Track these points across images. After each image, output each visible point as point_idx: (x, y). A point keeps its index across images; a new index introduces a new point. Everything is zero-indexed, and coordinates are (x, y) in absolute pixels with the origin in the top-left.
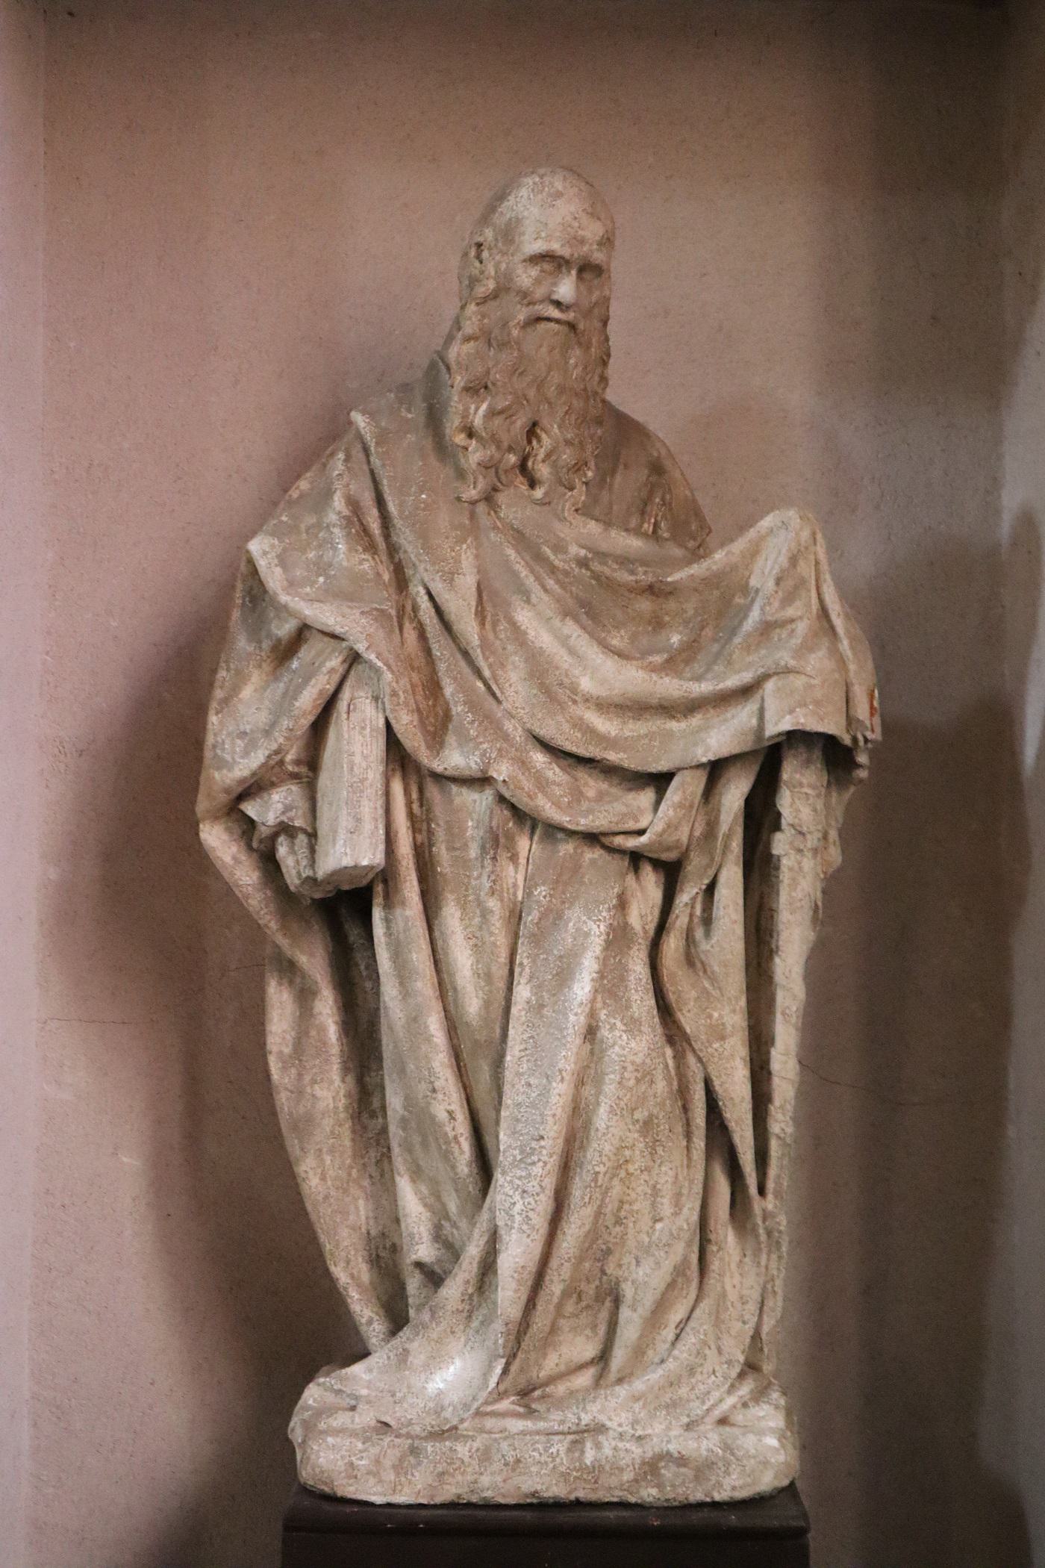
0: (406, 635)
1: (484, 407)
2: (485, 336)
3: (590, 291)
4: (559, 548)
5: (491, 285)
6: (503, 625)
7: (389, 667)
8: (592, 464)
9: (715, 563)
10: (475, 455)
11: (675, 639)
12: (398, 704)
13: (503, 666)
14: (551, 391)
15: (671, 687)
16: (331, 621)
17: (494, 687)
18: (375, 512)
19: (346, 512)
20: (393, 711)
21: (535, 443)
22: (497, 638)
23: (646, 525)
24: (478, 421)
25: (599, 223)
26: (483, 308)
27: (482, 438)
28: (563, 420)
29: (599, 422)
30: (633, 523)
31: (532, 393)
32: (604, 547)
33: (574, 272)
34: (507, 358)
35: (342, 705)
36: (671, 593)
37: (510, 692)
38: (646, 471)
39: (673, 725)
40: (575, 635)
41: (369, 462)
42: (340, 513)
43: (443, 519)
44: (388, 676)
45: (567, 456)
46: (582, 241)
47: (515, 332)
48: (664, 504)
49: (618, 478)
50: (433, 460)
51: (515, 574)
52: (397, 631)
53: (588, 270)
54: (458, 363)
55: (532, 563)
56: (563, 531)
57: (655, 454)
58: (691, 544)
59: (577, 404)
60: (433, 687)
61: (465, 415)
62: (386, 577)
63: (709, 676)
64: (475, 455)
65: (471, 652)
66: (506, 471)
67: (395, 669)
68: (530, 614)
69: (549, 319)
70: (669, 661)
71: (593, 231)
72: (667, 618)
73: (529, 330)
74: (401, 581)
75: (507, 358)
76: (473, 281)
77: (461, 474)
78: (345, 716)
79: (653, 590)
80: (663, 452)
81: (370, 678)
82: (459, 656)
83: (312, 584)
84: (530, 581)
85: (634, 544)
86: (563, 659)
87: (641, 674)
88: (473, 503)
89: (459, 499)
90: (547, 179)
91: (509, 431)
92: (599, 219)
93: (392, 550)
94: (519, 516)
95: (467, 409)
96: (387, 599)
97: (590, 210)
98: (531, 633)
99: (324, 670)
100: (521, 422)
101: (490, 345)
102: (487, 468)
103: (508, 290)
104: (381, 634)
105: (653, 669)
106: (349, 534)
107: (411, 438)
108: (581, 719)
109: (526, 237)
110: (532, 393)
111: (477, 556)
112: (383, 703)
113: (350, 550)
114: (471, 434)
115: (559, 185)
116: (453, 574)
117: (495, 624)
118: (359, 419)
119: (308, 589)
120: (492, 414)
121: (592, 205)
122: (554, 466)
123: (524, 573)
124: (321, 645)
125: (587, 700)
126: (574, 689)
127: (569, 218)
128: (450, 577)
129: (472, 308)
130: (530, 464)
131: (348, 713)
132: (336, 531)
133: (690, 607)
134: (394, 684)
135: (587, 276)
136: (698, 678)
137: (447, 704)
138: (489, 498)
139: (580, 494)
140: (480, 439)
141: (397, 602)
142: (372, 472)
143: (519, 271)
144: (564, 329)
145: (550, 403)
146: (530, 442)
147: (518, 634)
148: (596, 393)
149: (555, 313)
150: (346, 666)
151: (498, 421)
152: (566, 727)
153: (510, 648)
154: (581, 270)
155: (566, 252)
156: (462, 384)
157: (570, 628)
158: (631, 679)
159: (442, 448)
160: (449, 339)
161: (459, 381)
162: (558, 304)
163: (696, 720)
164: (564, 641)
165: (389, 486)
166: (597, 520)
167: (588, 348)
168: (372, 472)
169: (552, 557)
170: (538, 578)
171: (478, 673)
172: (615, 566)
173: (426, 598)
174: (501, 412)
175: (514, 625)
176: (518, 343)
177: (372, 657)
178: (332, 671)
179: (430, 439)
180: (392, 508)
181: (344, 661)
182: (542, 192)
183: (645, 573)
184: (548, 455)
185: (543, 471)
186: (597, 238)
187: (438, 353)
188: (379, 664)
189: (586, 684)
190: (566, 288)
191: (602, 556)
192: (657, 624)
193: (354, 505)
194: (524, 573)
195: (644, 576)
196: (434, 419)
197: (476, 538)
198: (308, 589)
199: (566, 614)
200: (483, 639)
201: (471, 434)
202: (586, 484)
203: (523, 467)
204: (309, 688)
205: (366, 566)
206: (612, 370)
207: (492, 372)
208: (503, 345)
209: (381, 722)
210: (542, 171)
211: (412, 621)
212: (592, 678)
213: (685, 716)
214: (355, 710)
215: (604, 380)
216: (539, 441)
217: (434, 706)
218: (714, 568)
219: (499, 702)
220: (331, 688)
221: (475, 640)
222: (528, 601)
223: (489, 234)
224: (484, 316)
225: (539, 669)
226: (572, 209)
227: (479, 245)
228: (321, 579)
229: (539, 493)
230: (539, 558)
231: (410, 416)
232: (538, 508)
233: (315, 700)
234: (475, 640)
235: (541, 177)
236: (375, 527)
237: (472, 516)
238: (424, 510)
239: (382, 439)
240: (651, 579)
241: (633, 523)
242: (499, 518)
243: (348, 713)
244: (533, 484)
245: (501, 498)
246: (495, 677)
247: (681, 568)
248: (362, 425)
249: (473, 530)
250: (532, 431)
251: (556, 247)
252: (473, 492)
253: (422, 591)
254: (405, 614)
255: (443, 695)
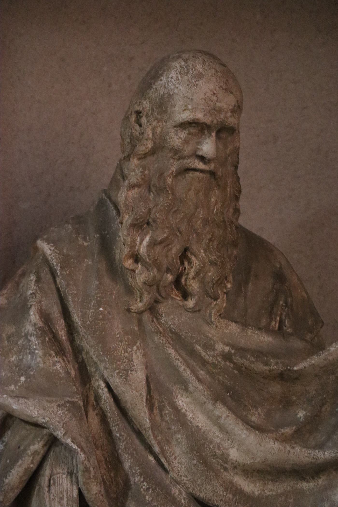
0: (90, 420)
1: (147, 239)
2: (147, 184)
3: (226, 147)
4: (208, 346)
5: (150, 145)
6: (168, 410)
7: (82, 449)
8: (231, 278)
9: (331, 354)
10: (141, 276)
11: (301, 414)
12: (90, 478)
13: (168, 442)
14: (198, 224)
15: (300, 454)
16: (35, 413)
17: (163, 460)
18: (62, 322)
19: (40, 324)
20: (84, 484)
21: (186, 264)
22: (163, 420)
23: (273, 323)
24: (143, 250)
25: (232, 96)
26: (145, 162)
27: (146, 262)
28: (208, 245)
29: (235, 244)
30: (264, 322)
31: (183, 227)
32: (243, 343)
33: (213, 134)
34: (163, 200)
35: (44, 480)
36: (297, 379)
37: (175, 463)
38: (272, 280)
39: (304, 485)
40: (224, 415)
41: (55, 282)
42: (35, 325)
43: (117, 326)
44: (82, 456)
45: (212, 274)
46: (220, 111)
47: (169, 180)
48: (287, 306)
49: (250, 286)
50: (107, 280)
51: (176, 369)
52: (85, 418)
53: (225, 132)
54: (126, 205)
55: (187, 358)
56: (211, 332)
57: (278, 266)
58: (309, 336)
59: (218, 232)
60: (113, 462)
61: (133, 245)
62: (73, 373)
63: (330, 444)
64: (141, 276)
65: (144, 432)
66: (165, 287)
67: (86, 449)
68: (188, 400)
69: (195, 170)
70: (297, 432)
71: (227, 102)
72: (294, 398)
73: (179, 178)
74: (84, 376)
75: (163, 200)
76: (134, 141)
77: (129, 290)
78: (47, 489)
79: (282, 377)
80: (283, 262)
81: (66, 458)
82: (134, 436)
83: (16, 382)
84: (187, 374)
85: (266, 340)
86: (215, 435)
87: (277, 445)
88: (140, 313)
89: (129, 310)
90: (190, 63)
91: (167, 256)
92: (231, 93)
93: (77, 351)
94: (176, 322)
95: (134, 241)
96: (76, 393)
97: (224, 87)
98: (190, 415)
99: (29, 452)
100: (175, 249)
101: (150, 190)
102: (150, 286)
103: (162, 148)
104: (74, 422)
105: (284, 439)
106: (43, 342)
107: (88, 262)
108: (231, 482)
109: (177, 109)
110: (183, 227)
111: (145, 355)
112: (77, 478)
113: (45, 354)
114: (137, 258)
115: (200, 68)
116: (127, 371)
117: (161, 410)
118: (45, 247)
119: (13, 387)
120: (153, 244)
121: (226, 83)
122: (202, 282)
123: (182, 367)
124: (24, 431)
125: (235, 467)
126: (225, 458)
127: (209, 94)
128: (125, 374)
129: (135, 162)
130: (183, 280)
131: (49, 486)
132: (33, 339)
133: (312, 389)
134: (86, 462)
135: (223, 135)
136: (321, 446)
137: (127, 475)
138: (152, 309)
139: (222, 303)
140: (144, 264)
141: (82, 393)
142: (58, 290)
143: (172, 134)
144: (208, 175)
145: (197, 234)
146: (182, 263)
147: (179, 416)
148: (232, 222)
149: (201, 165)
150: (46, 448)
151: (158, 249)
152: (220, 490)
153: (174, 428)
154: (219, 132)
155: (207, 120)
156: (130, 222)
157: (220, 410)
158: (268, 449)
159: (114, 270)
160: (115, 184)
161: (127, 219)
162: (202, 158)
163: (321, 481)
164: (215, 420)
165: (74, 302)
166: (236, 322)
167: (225, 189)
168: (58, 290)
169: (203, 354)
170: (193, 372)
171: (149, 449)
172: (253, 360)
173: (106, 390)
174: (161, 243)
175: (177, 410)
176: (172, 189)
177: (69, 441)
178: (35, 453)
179: (104, 263)
180: (76, 319)
181: (45, 445)
182: (187, 73)
183: (277, 364)
184: (197, 274)
185: (194, 286)
186: (231, 107)
187: (105, 191)
188: (75, 447)
189: (234, 454)
190: (208, 147)
191: (243, 351)
192: (287, 403)
193: (45, 317)
194: (182, 367)
195: (275, 366)
196: (106, 246)
197: (144, 340)
198: (13, 387)
199: (217, 398)
200: (152, 421)
201: (137, 258)
202: (226, 293)
203: (177, 282)
204: (16, 468)
205: (58, 366)
206: (243, 203)
207: (153, 212)
208: (161, 191)
209: (75, 493)
210: (186, 56)
211: (94, 410)
212: (238, 450)
213: (313, 478)
214: (54, 484)
215: (237, 211)
216: (190, 262)
217: (116, 476)
218: (330, 358)
219: (166, 471)
220: (33, 466)
221: (147, 423)
222: (186, 389)
223: (146, 104)
224: (144, 169)
225: (198, 445)
226: (212, 87)
227: (138, 113)
228: (23, 379)
229: (191, 303)
230: (193, 354)
231: (86, 244)
232: (191, 315)
233: (21, 477)
234: (147, 423)
235: (186, 61)
236: (62, 334)
237: (140, 323)
238: (102, 320)
239: (65, 262)
240: (281, 368)
241: (264, 322)
242: (160, 323)
243: (49, 486)
244: (185, 295)
245: (162, 308)
246: (163, 451)
247: (304, 359)
248: (49, 252)
249: (140, 335)
250: (184, 255)
251: (200, 116)
252: (140, 305)
253: (103, 385)
254: (89, 402)
255: (123, 468)
